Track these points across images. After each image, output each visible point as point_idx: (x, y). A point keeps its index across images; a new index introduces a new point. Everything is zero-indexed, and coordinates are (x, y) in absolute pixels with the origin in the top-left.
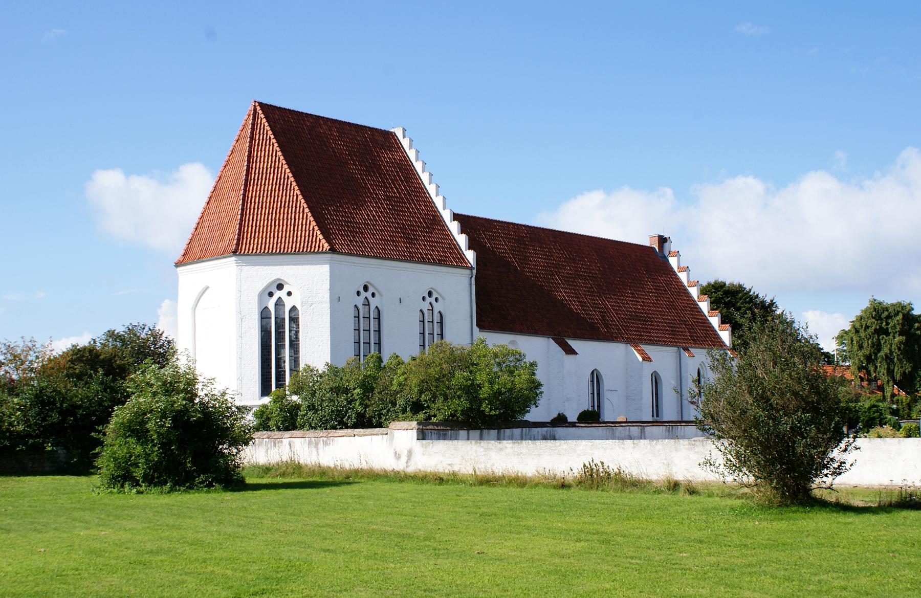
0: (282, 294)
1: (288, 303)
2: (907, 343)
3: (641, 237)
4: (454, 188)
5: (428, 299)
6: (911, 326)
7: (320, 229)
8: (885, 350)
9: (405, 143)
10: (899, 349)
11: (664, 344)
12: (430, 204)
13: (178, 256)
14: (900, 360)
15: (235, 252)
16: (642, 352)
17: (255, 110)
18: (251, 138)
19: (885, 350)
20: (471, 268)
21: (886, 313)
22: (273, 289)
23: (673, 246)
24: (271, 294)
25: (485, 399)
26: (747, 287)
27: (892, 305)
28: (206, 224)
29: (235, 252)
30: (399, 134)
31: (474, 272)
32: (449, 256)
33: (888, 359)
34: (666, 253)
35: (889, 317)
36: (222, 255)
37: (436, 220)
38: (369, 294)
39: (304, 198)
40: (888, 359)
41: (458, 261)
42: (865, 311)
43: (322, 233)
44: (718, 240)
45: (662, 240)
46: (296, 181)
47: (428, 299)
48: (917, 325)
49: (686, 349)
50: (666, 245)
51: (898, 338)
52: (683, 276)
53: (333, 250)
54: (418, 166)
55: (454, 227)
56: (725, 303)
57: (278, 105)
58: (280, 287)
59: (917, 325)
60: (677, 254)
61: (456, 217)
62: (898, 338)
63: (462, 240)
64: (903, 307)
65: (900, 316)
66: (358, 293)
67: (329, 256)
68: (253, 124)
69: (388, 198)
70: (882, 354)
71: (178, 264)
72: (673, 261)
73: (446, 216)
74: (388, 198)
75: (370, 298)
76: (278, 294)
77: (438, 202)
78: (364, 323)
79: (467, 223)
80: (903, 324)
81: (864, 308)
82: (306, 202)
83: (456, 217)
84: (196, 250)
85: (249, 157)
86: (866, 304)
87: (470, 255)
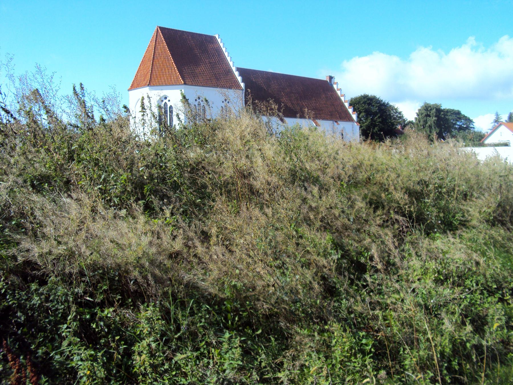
0: (166, 101)
1: (169, 104)
2: (437, 120)
3: (322, 75)
5: (198, 100)
6: (440, 114)
7: (181, 76)
8: (429, 123)
9: (219, 40)
10: (434, 123)
11: (327, 119)
12: (228, 65)
13: (129, 87)
14: (435, 128)
15: (148, 85)
16: (316, 123)
17: (157, 30)
18: (156, 41)
19: (429, 123)
20: (243, 90)
21: (430, 108)
22: (163, 99)
23: (336, 80)
24: (162, 101)
25: (475, 184)
26: (378, 97)
27: (433, 105)
28: (139, 74)
29: (148, 85)
30: (217, 37)
31: (244, 91)
32: (234, 85)
33: (430, 127)
34: (333, 83)
35: (431, 110)
36: (144, 86)
37: (229, 71)
38: (200, 101)
39: (175, 63)
40: (430, 127)
41: (238, 87)
42: (422, 107)
43: (181, 77)
44: (356, 78)
45: (331, 78)
46: (172, 57)
47: (198, 100)
48: (442, 113)
49: (336, 122)
50: (333, 80)
51: (434, 118)
52: (339, 93)
53: (185, 84)
54: (224, 50)
55: (237, 74)
56: (368, 104)
57: (167, 27)
58: (166, 98)
59: (442, 113)
60: (337, 83)
61: (238, 69)
62: (434, 118)
63: (239, 79)
64: (437, 106)
65: (435, 110)
66: (196, 100)
67: (184, 86)
68: (157, 35)
69: (210, 63)
70: (427, 125)
71: (129, 90)
72: (335, 86)
73: (234, 69)
74: (210, 63)
75: (201, 102)
76: (165, 101)
77: (231, 64)
79: (243, 72)
80: (436, 113)
81: (421, 105)
82: (176, 65)
83: (238, 69)
84: (136, 85)
85: (155, 48)
86: (422, 104)
87: (242, 85)
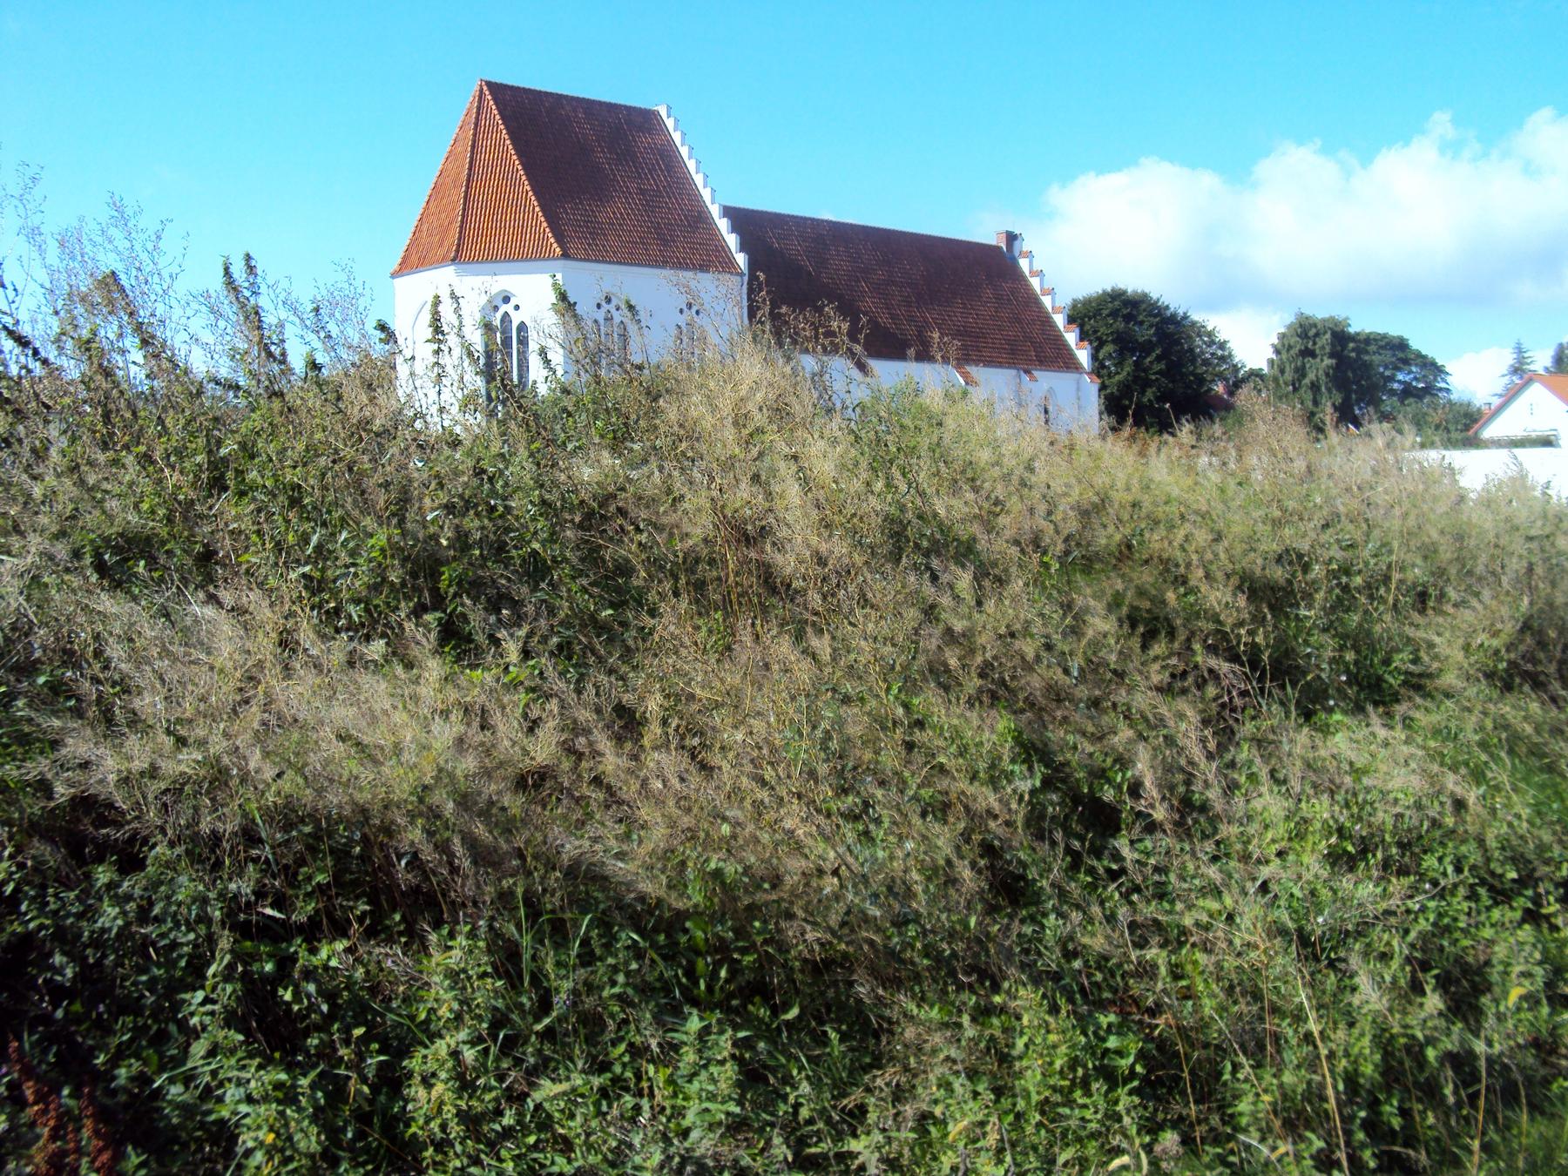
0: (509, 308)
1: (516, 319)
2: (1337, 368)
3: (984, 231)
4: (734, 167)
5: (605, 307)
6: (1344, 347)
7: (552, 231)
8: (1311, 376)
9: (670, 123)
10: (1327, 375)
11: (1000, 365)
12: (696, 197)
13: (395, 266)
14: (1329, 390)
15: (453, 260)
16: (965, 376)
17: (481, 90)
18: (476, 125)
19: (1311, 376)
20: (742, 274)
21: (1314, 331)
22: (498, 302)
23: (1026, 246)
24: (496, 308)
26: (1154, 296)
27: (1324, 320)
28: (425, 227)
29: (453, 260)
30: (663, 113)
31: (746, 279)
32: (715, 259)
33: (1315, 387)
34: (1017, 254)
35: (1317, 335)
36: (442, 262)
37: (700, 218)
38: (612, 307)
39: (535, 194)
40: (1315, 387)
41: (728, 265)
42: (1289, 327)
43: (555, 236)
44: (1089, 239)
45: (1011, 238)
46: (526, 174)
47: (605, 307)
48: (1351, 345)
49: (1027, 372)
50: (1016, 244)
51: (1328, 362)
52: (1035, 283)
53: (566, 255)
54: (684, 151)
55: (723, 225)
56: (1124, 317)
57: (510, 83)
58: (506, 300)
59: (1351, 345)
60: (1029, 255)
61: (728, 212)
62: (1328, 362)
63: (732, 240)
64: (1337, 323)
65: (1328, 336)
66: (599, 306)
67: (561, 263)
68: (478, 108)
69: (642, 192)
70: (1307, 381)
71: (394, 275)
72: (1024, 264)
73: (715, 211)
74: (642, 192)
75: (613, 310)
76: (504, 308)
77: (706, 194)
78: (597, 345)
79: (742, 220)
80: (1333, 345)
81: (1288, 322)
82: (538, 199)
83: (728, 212)
84: (414, 258)
85: (473, 147)
86: (1290, 318)
87: (741, 259)
